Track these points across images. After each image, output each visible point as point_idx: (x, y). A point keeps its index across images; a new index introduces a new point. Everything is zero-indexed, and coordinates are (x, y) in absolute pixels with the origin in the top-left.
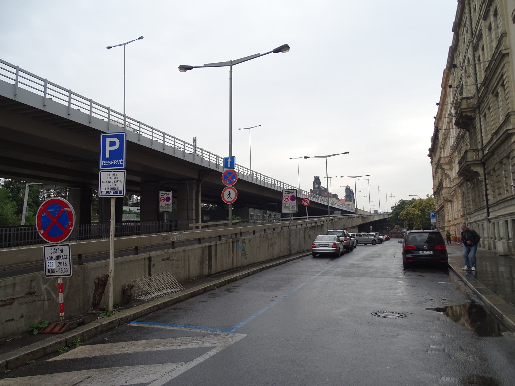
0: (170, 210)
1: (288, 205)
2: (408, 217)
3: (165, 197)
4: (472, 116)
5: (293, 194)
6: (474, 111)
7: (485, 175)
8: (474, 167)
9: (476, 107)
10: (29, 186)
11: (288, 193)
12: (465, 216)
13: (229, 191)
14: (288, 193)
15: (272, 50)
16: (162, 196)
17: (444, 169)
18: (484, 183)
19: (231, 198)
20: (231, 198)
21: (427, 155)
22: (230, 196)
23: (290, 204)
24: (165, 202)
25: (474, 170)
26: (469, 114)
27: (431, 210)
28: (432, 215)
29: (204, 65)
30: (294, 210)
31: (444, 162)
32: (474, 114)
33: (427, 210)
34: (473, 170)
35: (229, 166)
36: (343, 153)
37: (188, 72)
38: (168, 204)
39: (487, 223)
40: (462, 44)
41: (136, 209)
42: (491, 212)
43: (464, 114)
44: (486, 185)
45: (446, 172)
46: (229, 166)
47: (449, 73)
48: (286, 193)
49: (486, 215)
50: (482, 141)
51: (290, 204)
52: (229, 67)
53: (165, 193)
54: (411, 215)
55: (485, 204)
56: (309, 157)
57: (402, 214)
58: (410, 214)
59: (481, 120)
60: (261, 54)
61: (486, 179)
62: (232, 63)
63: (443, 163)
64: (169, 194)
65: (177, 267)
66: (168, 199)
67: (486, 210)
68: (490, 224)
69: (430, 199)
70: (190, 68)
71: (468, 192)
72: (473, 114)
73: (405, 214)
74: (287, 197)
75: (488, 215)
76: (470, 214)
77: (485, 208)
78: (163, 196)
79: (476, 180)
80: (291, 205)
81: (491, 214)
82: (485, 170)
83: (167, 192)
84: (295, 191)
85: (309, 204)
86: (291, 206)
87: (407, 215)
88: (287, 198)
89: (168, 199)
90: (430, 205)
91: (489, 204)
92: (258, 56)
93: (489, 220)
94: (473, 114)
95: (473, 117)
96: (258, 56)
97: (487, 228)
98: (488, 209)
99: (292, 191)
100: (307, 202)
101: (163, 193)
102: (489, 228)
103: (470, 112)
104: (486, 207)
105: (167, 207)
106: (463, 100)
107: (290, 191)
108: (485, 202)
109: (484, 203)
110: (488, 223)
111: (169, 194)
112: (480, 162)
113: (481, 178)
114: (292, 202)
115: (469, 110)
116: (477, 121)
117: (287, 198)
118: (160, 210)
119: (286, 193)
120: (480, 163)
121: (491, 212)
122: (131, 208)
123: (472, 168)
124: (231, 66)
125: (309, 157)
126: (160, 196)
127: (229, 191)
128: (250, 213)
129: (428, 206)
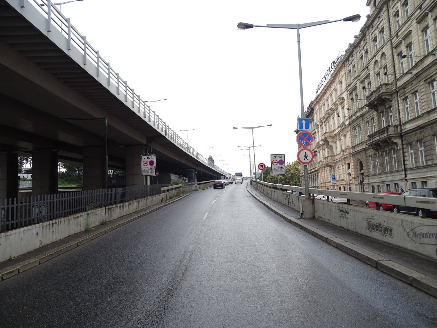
0: (154, 174)
1: (277, 168)
2: (273, 180)
3: (149, 160)
4: (389, 99)
6: (391, 95)
7: (403, 145)
8: (394, 139)
9: (395, 91)
11: (276, 157)
12: (359, 178)
13: (305, 153)
14: (276, 157)
15: (343, 19)
16: (145, 160)
17: (328, 141)
18: (401, 151)
19: (308, 160)
20: (308, 160)
22: (306, 157)
23: (278, 167)
24: (278, 165)
25: (395, 141)
26: (387, 97)
28: (333, 178)
29: (267, 25)
30: (283, 173)
31: (329, 136)
32: (391, 97)
34: (393, 141)
35: (304, 127)
36: (267, 126)
37: (247, 30)
38: (152, 167)
39: (404, 182)
40: (371, 43)
41: (29, 176)
42: (409, 174)
43: (384, 97)
44: (404, 153)
45: (329, 144)
46: (304, 127)
47: (343, 65)
49: (404, 176)
50: (400, 118)
51: (278, 167)
52: (297, 29)
53: (148, 156)
54: (276, 178)
55: (403, 168)
56: (237, 128)
57: (268, 178)
58: (274, 178)
59: (399, 102)
60: (330, 21)
61: (403, 149)
62: (299, 27)
63: (327, 137)
64: (153, 158)
66: (151, 163)
67: (403, 172)
68: (408, 183)
69: (289, 166)
70: (249, 26)
71: (367, 159)
72: (390, 97)
73: (271, 178)
74: (276, 161)
75: (406, 176)
76: (368, 177)
77: (403, 171)
78: (275, 159)
79: (388, 149)
81: (408, 176)
82: (402, 141)
83: (151, 156)
84: (283, 156)
85: (264, 168)
86: (280, 170)
87: (272, 179)
88: (275, 162)
89: (151, 163)
90: (290, 170)
91: (406, 167)
92: (327, 22)
93: (406, 180)
94: (390, 97)
95: (390, 99)
96: (327, 22)
97: (405, 186)
98: (405, 171)
100: (262, 167)
101: (146, 156)
102: (407, 186)
103: (389, 95)
104: (404, 170)
105: (280, 170)
106: (383, 86)
107: (279, 155)
108: (403, 166)
109: (402, 167)
110: (406, 182)
111: (153, 158)
112: (399, 135)
113: (400, 147)
115: (388, 94)
116: (394, 102)
117: (275, 162)
118: (143, 174)
119: (275, 158)
120: (399, 136)
121: (409, 174)
122: (25, 175)
123: (393, 140)
124: (298, 29)
125: (237, 128)
126: (143, 160)
127: (305, 153)
128: (171, 178)
129: (288, 171)
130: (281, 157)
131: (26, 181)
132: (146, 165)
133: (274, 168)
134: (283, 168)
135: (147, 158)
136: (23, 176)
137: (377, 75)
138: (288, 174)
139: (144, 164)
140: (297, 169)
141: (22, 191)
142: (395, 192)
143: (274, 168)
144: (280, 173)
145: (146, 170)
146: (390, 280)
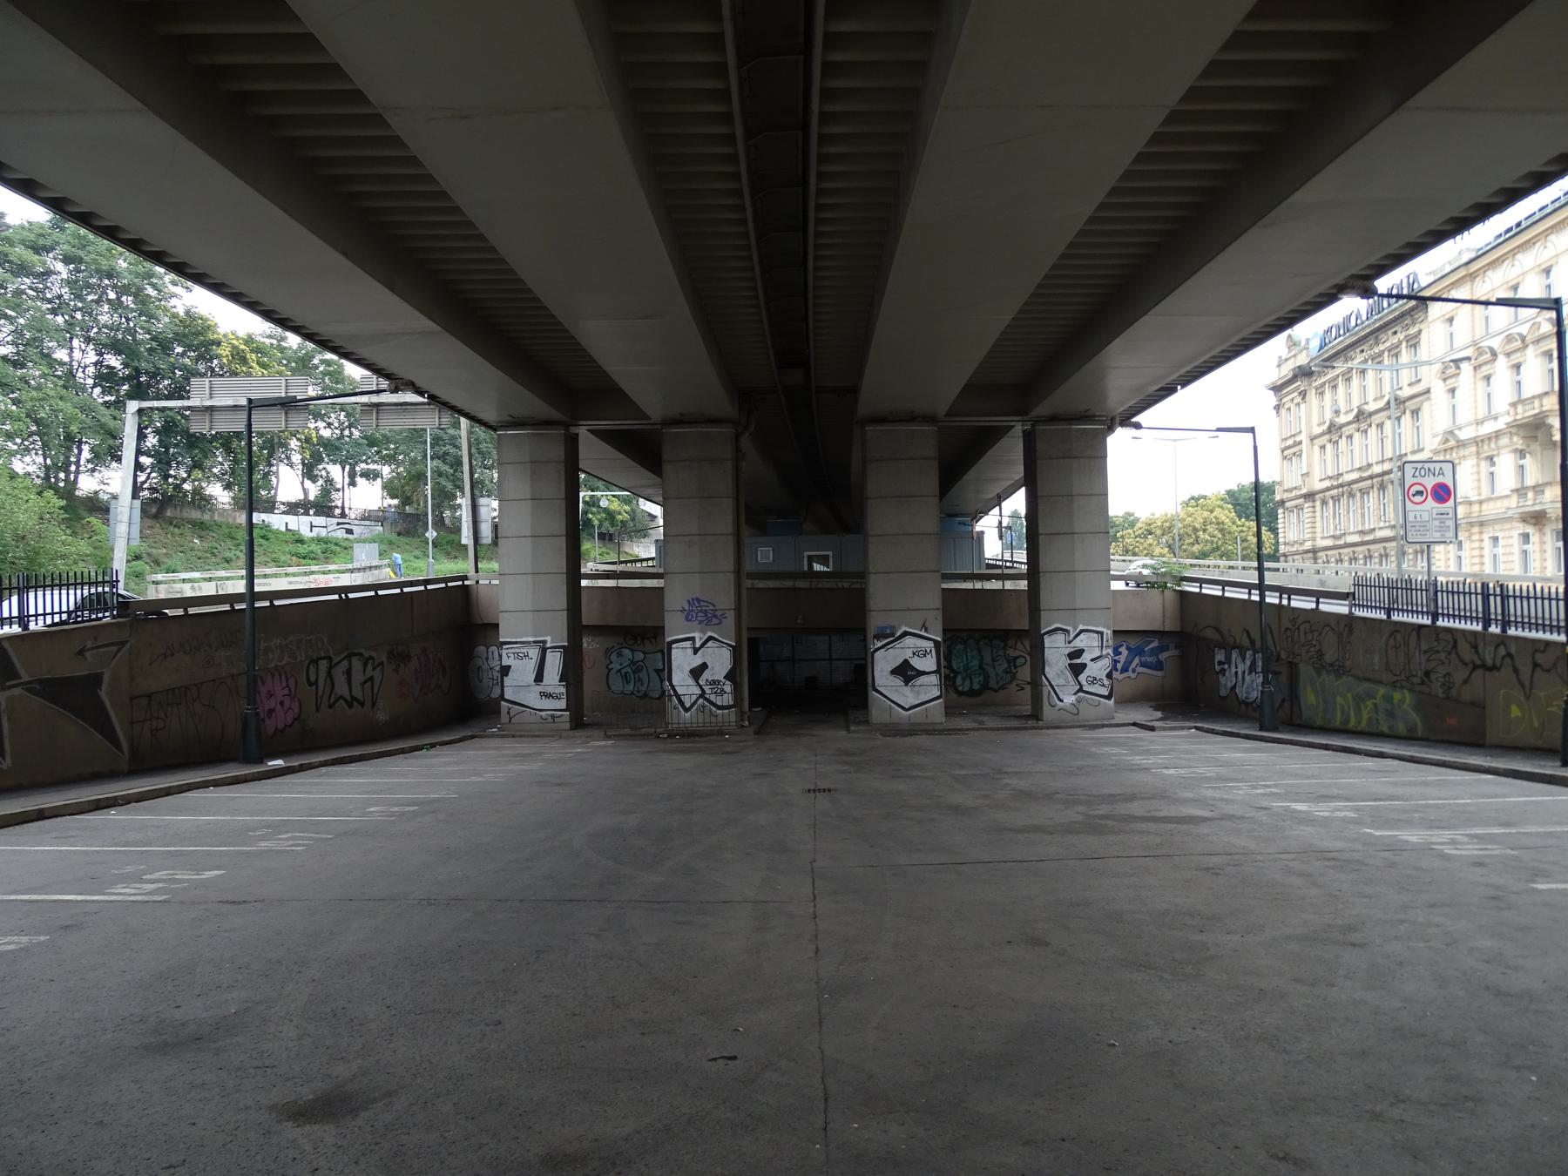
5: (1440, 479)
10: (140, 411)
16: (1415, 480)
21: (251, 331)
24: (1431, 503)
27: (1196, 546)
33: (1188, 544)
38: (1443, 511)
41: (818, 569)
48: (1417, 474)
65: (1126, 1150)
74: (1421, 488)
78: (1419, 480)
80: (1434, 519)
86: (1437, 523)
88: (1419, 493)
90: (1195, 530)
99: (1438, 466)
105: (1437, 523)
114: (1437, 505)
117: (1419, 493)
119: (1417, 474)
129: (1190, 532)
130: (1441, 473)
131: (110, 494)
132: (1418, 499)
133: (1415, 517)
134: (1450, 515)
135: (1423, 471)
136: (287, 524)
137: (1360, 372)
138: (1187, 541)
139: (1414, 495)
140: (1221, 526)
141: (990, 562)
142: (245, 410)
143: (1415, 517)
144: (1438, 534)
145: (1418, 519)
146: (511, 1156)
